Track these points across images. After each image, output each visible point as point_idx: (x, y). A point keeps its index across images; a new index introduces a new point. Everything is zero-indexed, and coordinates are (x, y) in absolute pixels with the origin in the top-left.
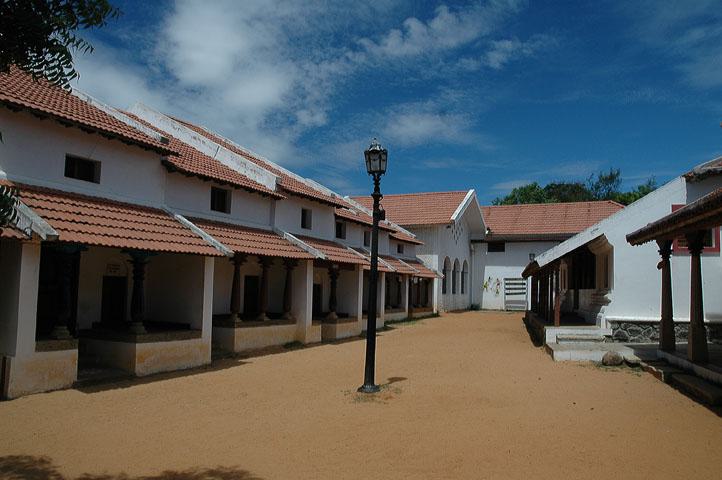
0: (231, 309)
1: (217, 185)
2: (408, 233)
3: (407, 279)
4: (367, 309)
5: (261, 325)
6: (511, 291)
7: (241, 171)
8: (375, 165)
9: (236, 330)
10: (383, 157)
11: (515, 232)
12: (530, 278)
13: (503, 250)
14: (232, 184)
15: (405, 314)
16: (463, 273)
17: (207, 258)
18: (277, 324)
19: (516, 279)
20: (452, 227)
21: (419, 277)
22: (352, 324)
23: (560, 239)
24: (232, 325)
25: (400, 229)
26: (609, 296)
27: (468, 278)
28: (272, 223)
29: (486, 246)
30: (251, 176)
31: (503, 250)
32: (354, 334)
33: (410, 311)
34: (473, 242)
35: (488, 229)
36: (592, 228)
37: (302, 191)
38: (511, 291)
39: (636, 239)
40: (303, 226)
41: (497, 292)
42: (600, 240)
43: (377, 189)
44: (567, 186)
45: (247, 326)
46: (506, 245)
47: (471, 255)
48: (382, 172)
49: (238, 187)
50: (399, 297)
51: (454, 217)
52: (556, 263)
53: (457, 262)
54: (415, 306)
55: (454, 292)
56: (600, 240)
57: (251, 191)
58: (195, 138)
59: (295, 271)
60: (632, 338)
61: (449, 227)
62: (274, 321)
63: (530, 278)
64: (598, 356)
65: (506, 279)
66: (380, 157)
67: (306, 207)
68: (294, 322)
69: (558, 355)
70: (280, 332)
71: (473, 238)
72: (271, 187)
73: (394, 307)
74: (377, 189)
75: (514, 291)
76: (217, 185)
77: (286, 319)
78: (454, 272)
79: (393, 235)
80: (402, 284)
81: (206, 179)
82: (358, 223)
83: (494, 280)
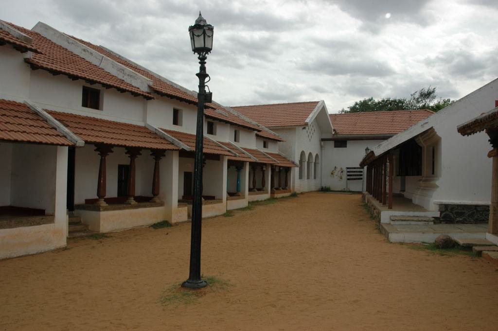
0: (98, 195)
1: (88, 85)
2: (273, 132)
3: (270, 169)
4: (29, 224)
5: (128, 208)
6: (352, 177)
7: (120, 77)
8: (199, 44)
9: (103, 214)
10: (208, 33)
11: (355, 133)
12: (366, 168)
13: (346, 147)
14: (104, 85)
15: (267, 196)
16: (315, 164)
17: (59, 147)
18: (145, 207)
19: (355, 168)
20: (307, 128)
21: (280, 167)
22: (216, 206)
23: (385, 138)
24: (98, 209)
25: (267, 129)
26: (438, 183)
27: (319, 166)
28: (145, 120)
29: (332, 143)
30: (128, 80)
31: (346, 147)
32: (218, 213)
33: (272, 193)
34: (323, 140)
35: (334, 130)
36: (423, 122)
37: (173, 93)
38: (352, 177)
39: (466, 130)
40: (176, 122)
41: (341, 178)
42: (430, 133)
43: (203, 68)
44: (392, 101)
45: (114, 209)
46: (348, 142)
47: (321, 150)
48: (208, 50)
49: (108, 87)
50: (263, 183)
51: (307, 120)
52: (388, 153)
53: (310, 154)
54: (277, 189)
55: (308, 178)
56: (430, 133)
57: (122, 91)
58: (84, 50)
59: (163, 162)
60: (458, 219)
61: (304, 128)
62: (142, 204)
63: (366, 168)
64: (430, 237)
65: (348, 168)
66: (204, 33)
67: (177, 107)
68: (162, 204)
69: (393, 237)
70: (146, 215)
71: (362, 180)
72: (144, 89)
73: (259, 190)
74: (203, 68)
75: (351, 170)
76: (88, 85)
77: (155, 202)
78: (309, 163)
79: (259, 133)
80: (265, 172)
81: (74, 78)
82: (227, 122)
83: (338, 169)
